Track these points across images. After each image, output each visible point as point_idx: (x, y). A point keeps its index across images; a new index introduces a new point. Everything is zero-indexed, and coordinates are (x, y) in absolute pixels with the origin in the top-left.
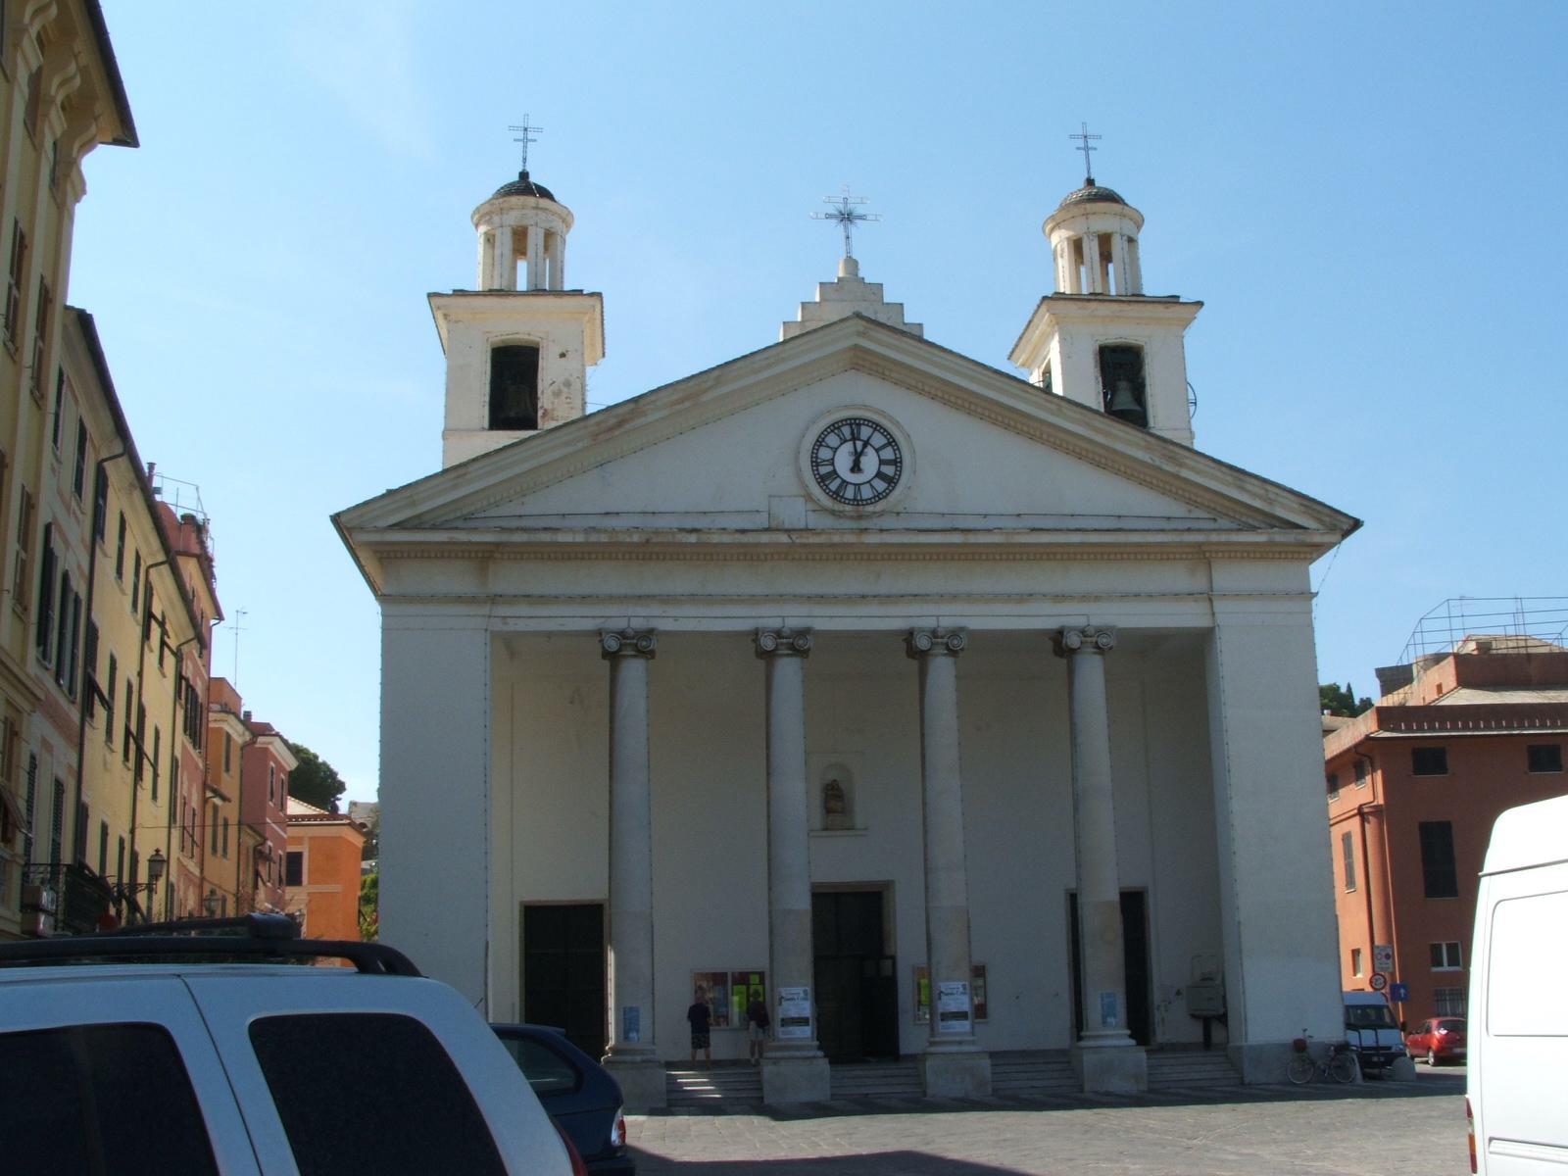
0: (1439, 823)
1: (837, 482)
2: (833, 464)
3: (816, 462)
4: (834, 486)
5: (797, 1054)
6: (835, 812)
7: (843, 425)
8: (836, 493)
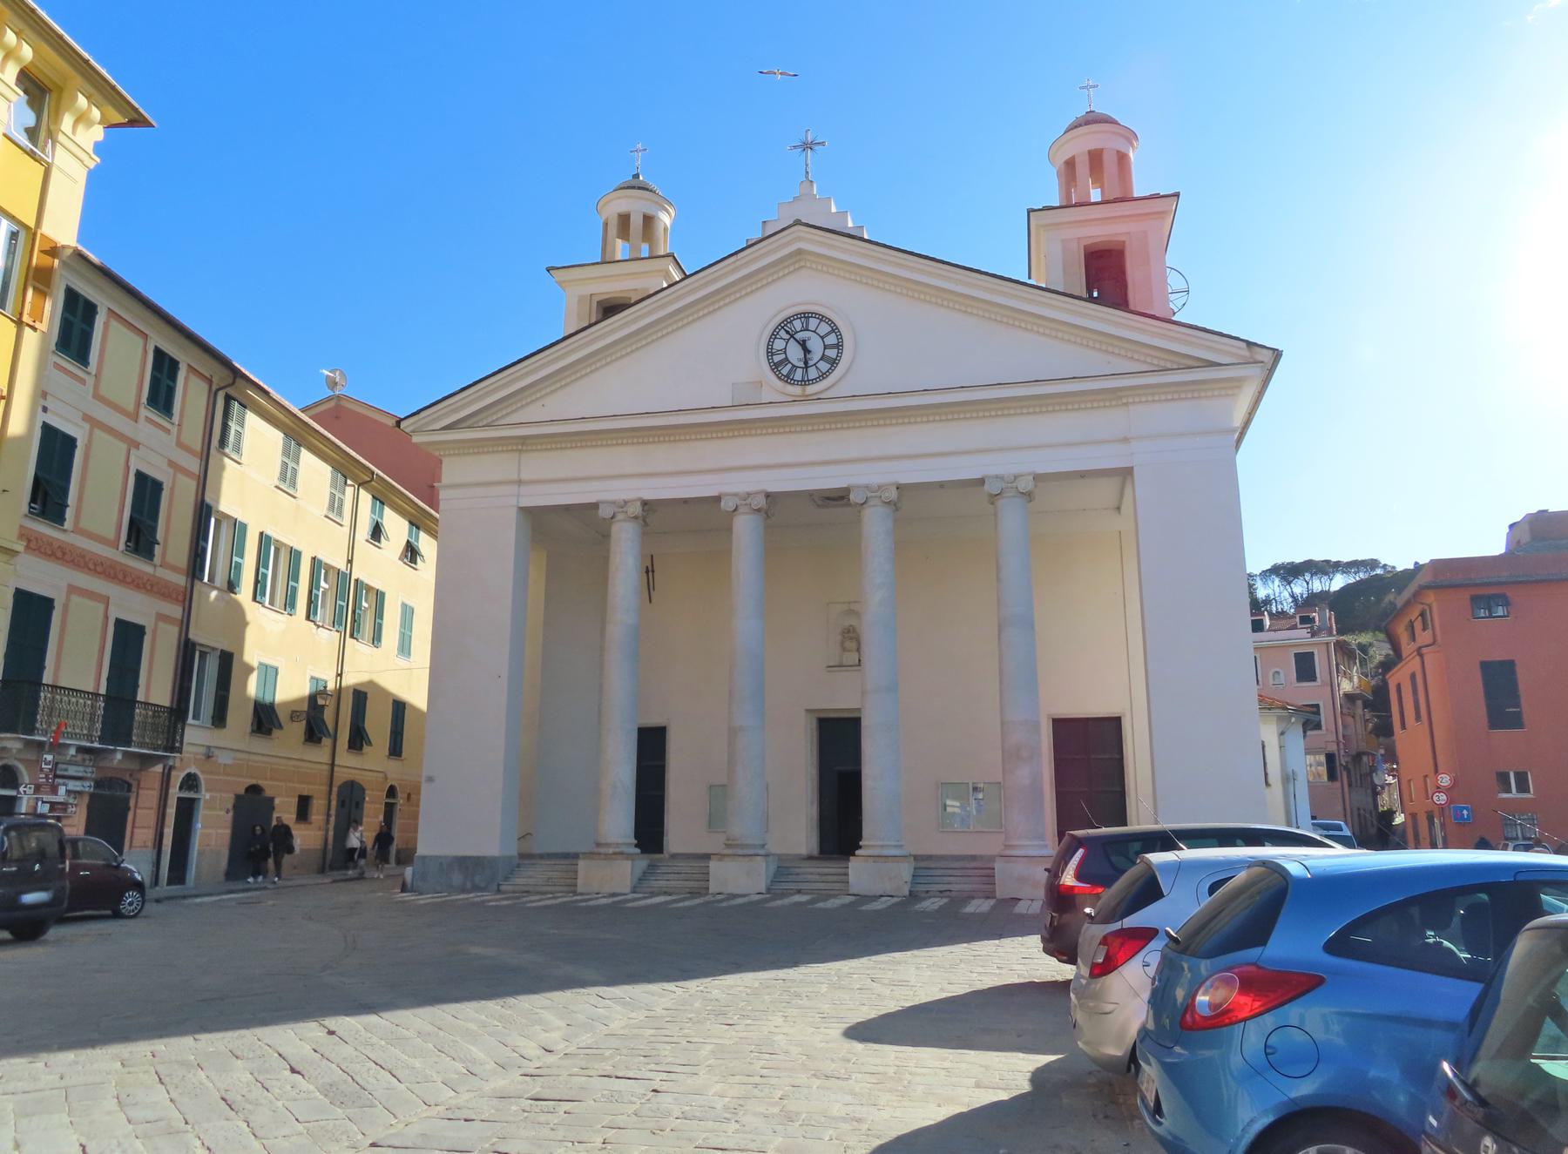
0: (1502, 663)
1: (789, 366)
2: (785, 353)
3: (771, 352)
4: (785, 371)
5: (740, 852)
6: (849, 651)
7: (795, 319)
8: (787, 376)
